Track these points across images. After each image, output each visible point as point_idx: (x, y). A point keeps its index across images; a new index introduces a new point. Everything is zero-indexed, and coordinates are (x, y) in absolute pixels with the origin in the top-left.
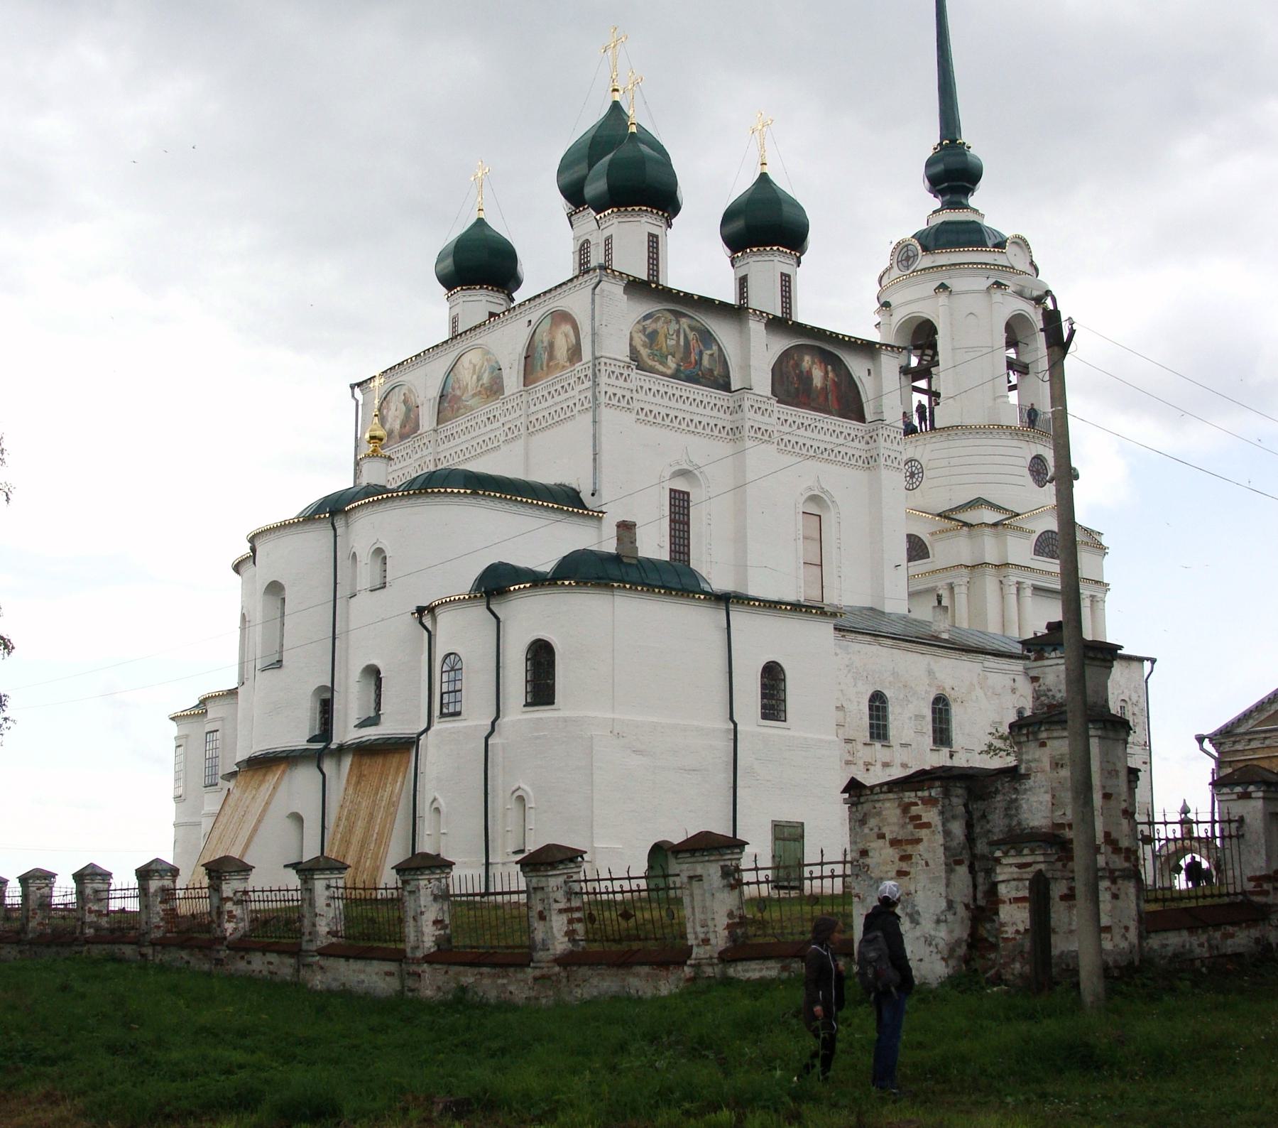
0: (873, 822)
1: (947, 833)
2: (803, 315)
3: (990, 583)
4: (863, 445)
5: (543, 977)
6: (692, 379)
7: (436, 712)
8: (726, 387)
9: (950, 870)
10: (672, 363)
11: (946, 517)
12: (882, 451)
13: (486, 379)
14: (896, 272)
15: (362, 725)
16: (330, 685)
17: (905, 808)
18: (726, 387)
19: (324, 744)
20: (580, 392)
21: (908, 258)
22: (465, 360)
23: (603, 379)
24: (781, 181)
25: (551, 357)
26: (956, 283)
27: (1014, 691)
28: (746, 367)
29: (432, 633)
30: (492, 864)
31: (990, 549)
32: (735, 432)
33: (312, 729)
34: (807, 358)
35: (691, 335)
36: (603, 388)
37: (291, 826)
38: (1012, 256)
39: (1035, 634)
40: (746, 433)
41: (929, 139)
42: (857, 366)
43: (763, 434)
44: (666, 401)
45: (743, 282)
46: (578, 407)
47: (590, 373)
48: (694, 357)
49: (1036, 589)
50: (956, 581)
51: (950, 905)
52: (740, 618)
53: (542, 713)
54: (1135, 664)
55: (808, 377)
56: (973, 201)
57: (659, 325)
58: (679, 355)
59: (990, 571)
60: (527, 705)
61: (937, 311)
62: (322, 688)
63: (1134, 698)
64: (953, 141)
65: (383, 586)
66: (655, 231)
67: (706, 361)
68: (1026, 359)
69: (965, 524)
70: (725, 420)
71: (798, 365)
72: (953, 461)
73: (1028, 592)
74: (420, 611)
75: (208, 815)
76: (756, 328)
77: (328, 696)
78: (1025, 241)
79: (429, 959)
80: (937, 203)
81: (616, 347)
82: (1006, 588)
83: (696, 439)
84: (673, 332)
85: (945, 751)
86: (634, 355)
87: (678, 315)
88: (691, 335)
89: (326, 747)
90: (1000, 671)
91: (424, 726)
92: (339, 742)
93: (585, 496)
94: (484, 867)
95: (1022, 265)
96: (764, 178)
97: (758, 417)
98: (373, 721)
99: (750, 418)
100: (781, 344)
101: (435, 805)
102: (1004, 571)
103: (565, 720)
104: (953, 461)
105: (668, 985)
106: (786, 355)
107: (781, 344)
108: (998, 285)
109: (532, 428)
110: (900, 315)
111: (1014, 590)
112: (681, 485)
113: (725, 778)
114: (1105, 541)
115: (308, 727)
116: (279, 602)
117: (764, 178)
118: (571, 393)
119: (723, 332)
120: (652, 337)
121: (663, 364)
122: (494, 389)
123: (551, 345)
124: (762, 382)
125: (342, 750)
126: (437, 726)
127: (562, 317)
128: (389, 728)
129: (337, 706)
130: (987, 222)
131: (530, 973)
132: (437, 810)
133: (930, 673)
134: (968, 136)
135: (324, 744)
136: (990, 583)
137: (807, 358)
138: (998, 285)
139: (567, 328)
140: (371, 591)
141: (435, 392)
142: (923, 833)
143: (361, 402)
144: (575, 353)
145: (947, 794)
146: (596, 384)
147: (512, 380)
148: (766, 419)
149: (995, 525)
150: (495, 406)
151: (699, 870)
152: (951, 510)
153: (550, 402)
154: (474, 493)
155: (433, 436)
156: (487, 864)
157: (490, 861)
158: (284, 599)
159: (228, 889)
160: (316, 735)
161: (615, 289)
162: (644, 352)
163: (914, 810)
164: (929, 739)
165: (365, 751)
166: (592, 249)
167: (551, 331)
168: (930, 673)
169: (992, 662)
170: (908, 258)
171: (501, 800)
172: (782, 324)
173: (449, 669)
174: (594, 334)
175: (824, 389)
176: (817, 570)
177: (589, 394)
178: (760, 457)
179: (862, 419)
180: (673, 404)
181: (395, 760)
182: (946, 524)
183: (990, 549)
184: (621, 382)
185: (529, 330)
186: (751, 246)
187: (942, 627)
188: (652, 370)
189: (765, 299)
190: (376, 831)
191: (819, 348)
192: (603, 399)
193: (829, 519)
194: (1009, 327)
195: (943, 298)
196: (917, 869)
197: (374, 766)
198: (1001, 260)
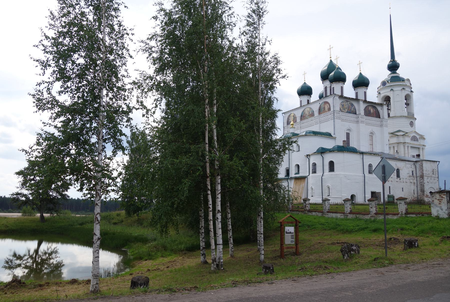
0: (434, 197)
1: (447, 199)
2: (368, 100)
3: (402, 146)
4: (380, 123)
5: (372, 216)
6: (349, 113)
7: (311, 172)
8: (356, 114)
9: (447, 204)
10: (346, 110)
11: (393, 134)
12: (384, 124)
13: (311, 113)
14: (382, 87)
15: (295, 174)
17: (440, 196)
18: (356, 114)
20: (331, 116)
21: (384, 84)
22: (306, 110)
23: (335, 114)
24: (364, 74)
25: (324, 110)
26: (395, 89)
27: (411, 167)
28: (359, 110)
31: (401, 140)
32: (357, 122)
34: (370, 107)
35: (349, 105)
36: (335, 116)
38: (407, 83)
40: (360, 122)
41: (388, 60)
42: (379, 108)
43: (362, 122)
44: (345, 117)
45: (357, 94)
46: (330, 119)
47: (333, 113)
48: (350, 109)
49: (411, 147)
50: (395, 146)
51: (448, 208)
52: (365, 157)
53: (332, 173)
54: (436, 162)
55: (370, 111)
56: (397, 72)
57: (344, 103)
58: (348, 108)
59: (402, 144)
61: (391, 94)
62: (287, 168)
63: (435, 169)
64: (394, 60)
65: (299, 151)
66: (342, 86)
67: (352, 109)
68: (408, 102)
69: (397, 135)
70: (356, 120)
71: (368, 109)
72: (394, 123)
73: (410, 148)
74: (307, 155)
76: (361, 103)
77: (288, 169)
78: (409, 79)
79: (349, 213)
80: (390, 72)
81: (338, 108)
82: (405, 147)
83: (351, 123)
84: (347, 104)
85: (399, 179)
86: (340, 110)
87: (347, 101)
88: (349, 105)
90: (409, 164)
93: (332, 135)
95: (408, 84)
96: (361, 74)
97: (362, 119)
98: (298, 173)
99: (360, 119)
100: (366, 105)
102: (405, 144)
103: (336, 174)
104: (394, 123)
105: (395, 217)
106: (366, 107)
107: (366, 105)
108: (404, 89)
109: (321, 122)
110: (382, 95)
111: (407, 147)
112: (348, 132)
113: (363, 184)
114: (425, 137)
117: (361, 74)
118: (328, 116)
119: (355, 104)
120: (343, 105)
121: (345, 110)
122: (312, 115)
123: (324, 108)
124: (362, 112)
125: (291, 178)
126: (311, 175)
127: (326, 103)
128: (301, 175)
129: (290, 171)
130: (400, 76)
131: (370, 215)
132: (312, 189)
133: (396, 165)
134: (397, 59)
136: (402, 146)
137: (370, 107)
138: (404, 89)
139: (328, 105)
141: (300, 115)
142: (443, 199)
144: (329, 109)
145: (447, 194)
146: (334, 115)
147: (316, 114)
148: (363, 119)
149: (403, 135)
150: (313, 118)
151: (401, 202)
152: (394, 132)
153: (324, 118)
154: (315, 135)
155: (300, 123)
159: (307, 203)
161: (337, 98)
162: (342, 108)
163: (442, 196)
164: (396, 176)
165: (296, 179)
166: (328, 88)
167: (324, 105)
168: (396, 165)
169: (407, 162)
170: (384, 84)
171: (325, 187)
172: (365, 101)
174: (333, 106)
175: (373, 113)
176: (372, 146)
177: (333, 117)
178: (362, 126)
179: (380, 118)
180: (347, 117)
181: (303, 180)
182: (393, 135)
183: (401, 140)
184: (338, 114)
185: (320, 105)
186: (358, 87)
187: (397, 156)
188: (343, 112)
189: (361, 97)
191: (373, 106)
192: (335, 117)
193: (374, 137)
194: (405, 97)
195: (392, 92)
196: (442, 203)
197: (298, 182)
198: (404, 84)
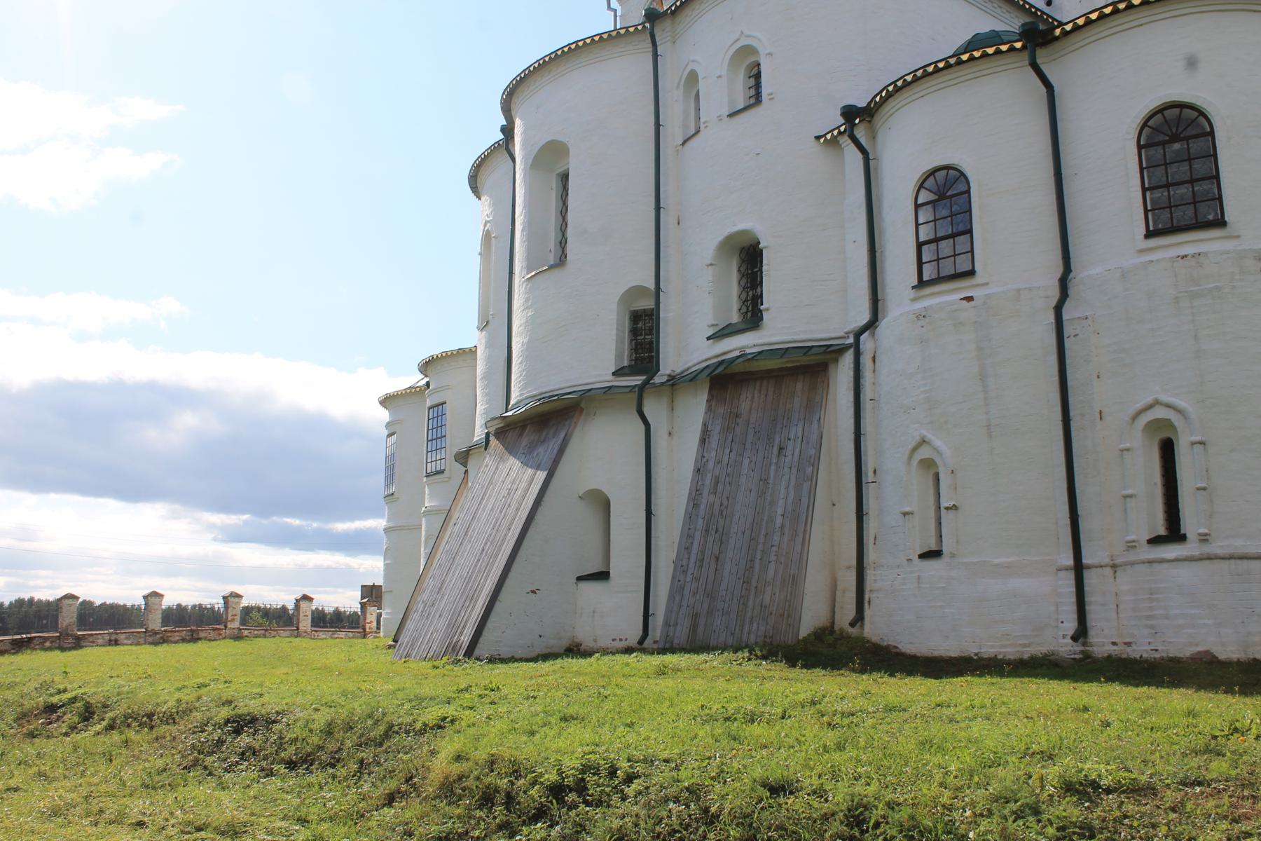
16: (652, 286)
19: (644, 378)
29: (871, 157)
30: (1089, 567)
33: (619, 357)
37: (588, 518)
39: (864, 434)
60: (1149, 234)
62: (637, 291)
75: (428, 513)
77: (646, 304)
89: (646, 383)
91: (864, 317)
92: (668, 372)
94: (1071, 576)
101: (924, 453)
115: (614, 352)
116: (554, 183)
135: (644, 378)
140: (731, 115)
143: (619, 13)
156: (1079, 568)
157: (1084, 561)
158: (565, 177)
160: (624, 367)
173: (932, 197)
190: (780, 511)
